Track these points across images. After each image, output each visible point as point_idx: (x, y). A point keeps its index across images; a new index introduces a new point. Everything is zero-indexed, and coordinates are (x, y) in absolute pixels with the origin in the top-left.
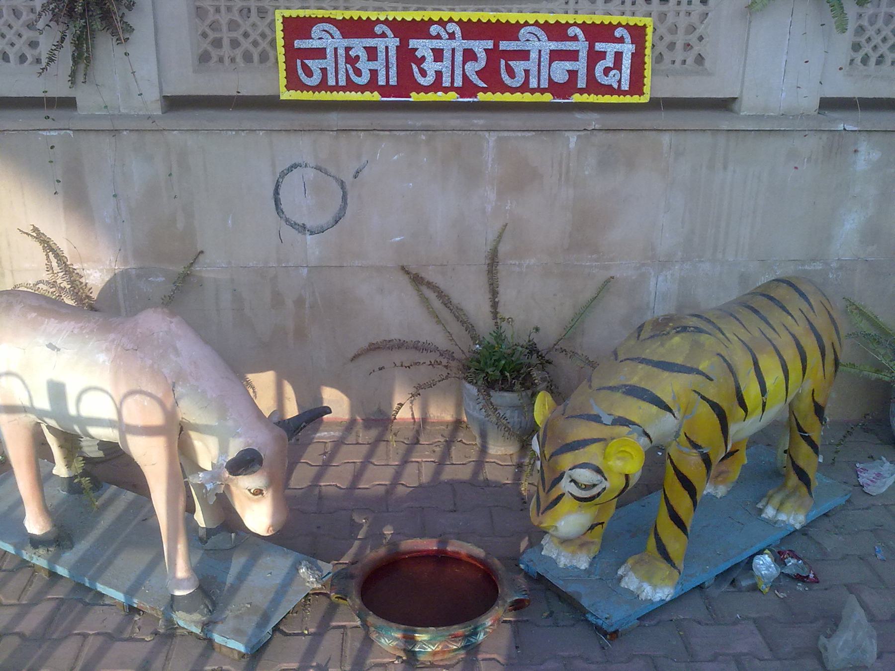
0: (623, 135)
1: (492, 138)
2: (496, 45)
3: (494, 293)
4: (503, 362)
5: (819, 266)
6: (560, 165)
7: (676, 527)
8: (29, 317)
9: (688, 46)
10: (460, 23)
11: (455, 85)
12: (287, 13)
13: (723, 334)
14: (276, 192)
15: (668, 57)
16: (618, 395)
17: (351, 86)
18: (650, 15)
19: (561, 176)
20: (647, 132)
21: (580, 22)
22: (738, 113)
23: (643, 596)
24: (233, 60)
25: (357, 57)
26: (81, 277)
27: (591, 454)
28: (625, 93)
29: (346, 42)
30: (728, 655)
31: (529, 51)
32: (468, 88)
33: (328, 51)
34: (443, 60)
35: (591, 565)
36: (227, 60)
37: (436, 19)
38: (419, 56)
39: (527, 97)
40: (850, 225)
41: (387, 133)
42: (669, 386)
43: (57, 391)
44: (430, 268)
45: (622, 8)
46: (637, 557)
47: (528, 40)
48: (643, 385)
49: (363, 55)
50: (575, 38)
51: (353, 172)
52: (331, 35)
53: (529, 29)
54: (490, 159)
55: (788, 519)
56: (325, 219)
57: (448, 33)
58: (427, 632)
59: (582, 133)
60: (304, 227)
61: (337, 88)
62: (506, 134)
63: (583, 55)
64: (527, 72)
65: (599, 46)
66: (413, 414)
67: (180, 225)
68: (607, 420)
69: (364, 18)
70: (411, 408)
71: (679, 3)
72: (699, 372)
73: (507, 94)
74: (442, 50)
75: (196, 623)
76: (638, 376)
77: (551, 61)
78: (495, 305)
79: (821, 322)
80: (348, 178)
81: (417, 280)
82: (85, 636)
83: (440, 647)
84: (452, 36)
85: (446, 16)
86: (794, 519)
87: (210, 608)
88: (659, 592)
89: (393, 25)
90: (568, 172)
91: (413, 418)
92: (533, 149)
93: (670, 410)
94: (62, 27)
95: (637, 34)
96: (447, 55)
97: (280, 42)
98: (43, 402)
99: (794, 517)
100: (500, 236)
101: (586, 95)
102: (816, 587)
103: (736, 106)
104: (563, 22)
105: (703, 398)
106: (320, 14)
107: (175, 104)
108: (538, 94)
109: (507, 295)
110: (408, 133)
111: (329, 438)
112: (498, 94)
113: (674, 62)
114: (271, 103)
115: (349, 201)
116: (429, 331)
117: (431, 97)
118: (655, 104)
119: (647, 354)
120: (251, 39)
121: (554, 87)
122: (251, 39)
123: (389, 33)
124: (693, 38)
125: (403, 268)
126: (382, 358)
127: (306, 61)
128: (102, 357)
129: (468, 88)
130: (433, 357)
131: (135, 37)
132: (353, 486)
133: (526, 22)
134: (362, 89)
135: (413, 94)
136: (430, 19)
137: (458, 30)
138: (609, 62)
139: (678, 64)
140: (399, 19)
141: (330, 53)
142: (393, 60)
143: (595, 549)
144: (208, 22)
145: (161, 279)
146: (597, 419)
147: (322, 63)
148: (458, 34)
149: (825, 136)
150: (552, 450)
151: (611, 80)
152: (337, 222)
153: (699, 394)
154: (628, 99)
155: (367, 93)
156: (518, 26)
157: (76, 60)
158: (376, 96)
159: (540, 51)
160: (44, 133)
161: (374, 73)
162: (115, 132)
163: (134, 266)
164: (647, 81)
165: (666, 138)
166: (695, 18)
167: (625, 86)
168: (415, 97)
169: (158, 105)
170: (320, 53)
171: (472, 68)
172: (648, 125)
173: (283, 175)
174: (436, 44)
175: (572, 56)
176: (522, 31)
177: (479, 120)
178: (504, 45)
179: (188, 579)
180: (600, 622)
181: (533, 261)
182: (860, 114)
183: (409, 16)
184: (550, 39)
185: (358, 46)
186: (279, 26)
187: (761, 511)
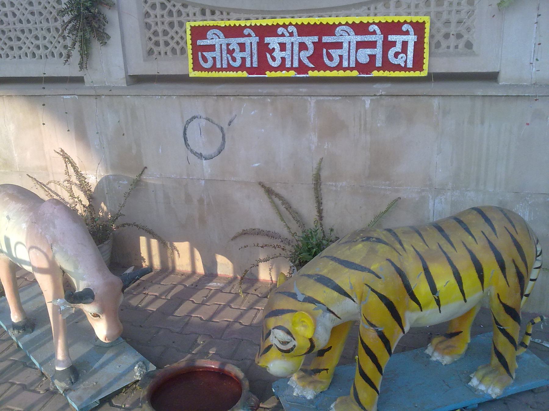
0: (403, 99)
1: (312, 101)
2: (320, 39)
3: (319, 203)
4: (315, 250)
6: (360, 120)
7: (364, 382)
9: (459, 36)
10: (296, 25)
11: (294, 66)
12: (193, 24)
13: (401, 245)
14: (185, 134)
15: (444, 44)
16: (311, 281)
17: (230, 68)
19: (360, 125)
21: (377, 21)
22: (498, 83)
25: (234, 50)
26: (86, 179)
27: (285, 320)
28: (409, 70)
31: (342, 42)
32: (302, 68)
34: (287, 50)
35: (316, 397)
37: (281, 23)
38: (271, 48)
39: (341, 74)
41: (247, 97)
42: (347, 279)
44: (278, 184)
46: (344, 397)
47: (341, 35)
48: (329, 276)
49: (237, 49)
50: (374, 33)
51: (228, 122)
54: (312, 115)
55: (487, 390)
56: (213, 150)
57: (289, 32)
59: (374, 98)
61: (222, 69)
62: (322, 98)
63: (380, 44)
64: (341, 57)
65: (391, 38)
66: (271, 278)
67: (134, 151)
68: (300, 297)
70: (270, 274)
71: (451, 4)
72: (370, 271)
73: (328, 72)
74: (285, 44)
75: (62, 387)
78: (320, 211)
79: (503, 243)
80: (225, 127)
82: (13, 384)
84: (291, 34)
85: (287, 21)
86: (492, 390)
87: (73, 381)
89: (255, 28)
90: (365, 124)
91: (272, 280)
92: (341, 108)
93: (349, 297)
95: (419, 28)
96: (288, 47)
97: (189, 42)
101: (381, 72)
104: (365, 22)
105: (373, 290)
106: (211, 23)
107: (138, 80)
108: (348, 72)
109: (328, 205)
111: (215, 287)
112: (322, 71)
114: (184, 79)
117: (279, 74)
118: (436, 77)
120: (175, 41)
121: (359, 67)
122: (175, 41)
123: (253, 34)
125: (260, 183)
126: (250, 240)
127: (204, 53)
129: (302, 68)
132: (210, 319)
133: (340, 23)
134: (236, 69)
135: (268, 73)
137: (295, 30)
138: (398, 48)
139: (452, 49)
140: (258, 25)
141: (217, 47)
142: (255, 51)
143: (322, 387)
144: (152, 31)
145: (126, 182)
146: (294, 296)
147: (213, 54)
148: (295, 33)
151: (400, 61)
152: (220, 153)
153: (368, 286)
154: (412, 74)
155: (240, 72)
156: (335, 26)
158: (245, 74)
159: (349, 42)
160: (65, 97)
161: (243, 59)
162: (97, 96)
164: (426, 61)
165: (436, 102)
167: (410, 65)
168: (268, 74)
169: (125, 81)
170: (211, 48)
171: (304, 55)
172: (420, 92)
173: (188, 123)
174: (281, 40)
175: (373, 45)
176: (338, 29)
177: (303, 89)
178: (326, 39)
179: (63, 361)
181: (344, 183)
183: (264, 23)
184: (356, 34)
185: (234, 42)
186: (189, 32)
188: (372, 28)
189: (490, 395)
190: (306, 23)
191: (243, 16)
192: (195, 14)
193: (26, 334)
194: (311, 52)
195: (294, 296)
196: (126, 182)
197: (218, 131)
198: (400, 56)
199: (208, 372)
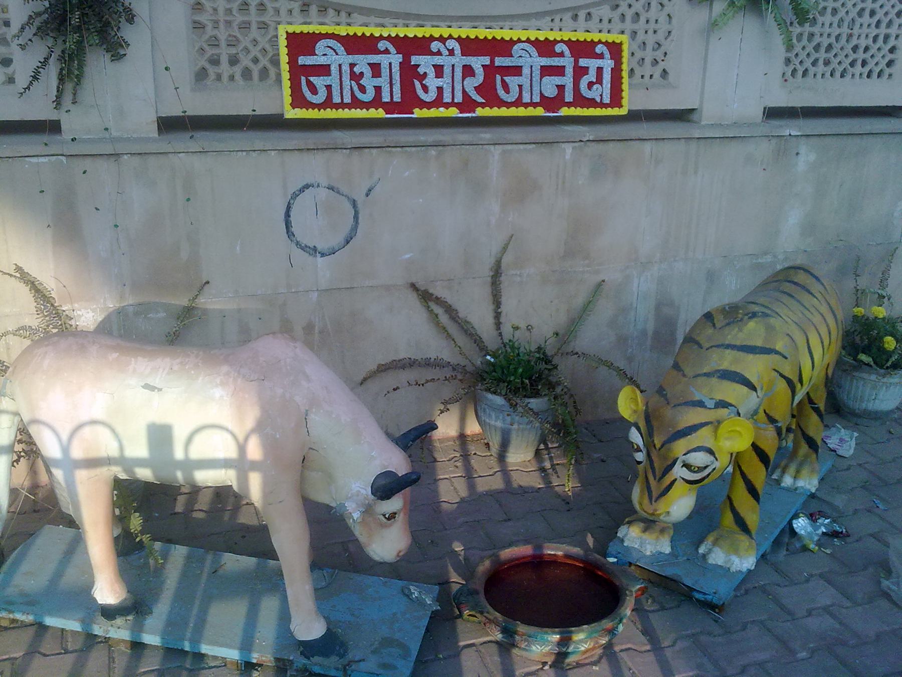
2: (492, 61)
3: (497, 303)
5: (769, 258)
8: (110, 358)
10: (459, 39)
11: (456, 101)
12: (291, 29)
14: (287, 215)
16: (714, 380)
17: (356, 103)
18: (623, 32)
20: (633, 142)
21: (566, 39)
23: (733, 569)
24: (232, 78)
25: (362, 74)
27: (703, 437)
29: (351, 59)
30: (819, 608)
33: (332, 68)
34: (446, 78)
36: (225, 78)
37: (437, 36)
40: (793, 219)
41: (399, 149)
42: (755, 367)
43: (160, 435)
45: (600, 26)
48: (733, 369)
49: (368, 72)
50: (561, 55)
51: (365, 191)
52: (335, 50)
53: (522, 45)
56: (336, 239)
58: (583, 631)
60: (315, 249)
61: (342, 106)
62: (509, 147)
63: (569, 71)
65: (583, 62)
68: (710, 404)
69: (359, 34)
74: (443, 66)
76: (727, 360)
77: (542, 77)
78: (497, 315)
80: (360, 198)
81: (426, 297)
83: (592, 644)
84: (451, 52)
86: (809, 484)
88: (744, 562)
89: (395, 41)
94: (50, 42)
95: (615, 49)
96: (447, 71)
97: (284, 59)
98: (139, 449)
99: (809, 483)
100: (505, 249)
102: (848, 540)
103: (695, 117)
104: (552, 39)
105: (782, 375)
106: (324, 29)
107: (169, 125)
108: (531, 109)
109: (509, 305)
110: (419, 148)
112: (496, 108)
113: (642, 77)
115: (360, 218)
116: (436, 348)
117: (433, 113)
118: (634, 116)
119: (729, 340)
123: (392, 49)
124: (659, 55)
127: (312, 79)
128: (218, 392)
129: (467, 104)
130: (448, 372)
131: (130, 51)
133: (519, 39)
135: (416, 110)
136: (431, 35)
138: (592, 76)
140: (402, 35)
141: (334, 69)
145: (162, 315)
146: (701, 404)
147: (327, 80)
148: (458, 51)
149: (774, 141)
150: (664, 439)
152: (348, 243)
155: (372, 110)
156: (512, 43)
157: (61, 79)
158: (380, 113)
162: (116, 156)
163: (131, 302)
164: (625, 94)
165: (647, 147)
166: (660, 36)
167: (607, 100)
168: (418, 113)
170: (324, 70)
172: (634, 135)
173: (295, 196)
174: (437, 60)
175: (559, 71)
176: (515, 47)
178: (499, 61)
180: (709, 598)
182: (801, 122)
183: (411, 32)
185: (363, 62)
186: (283, 42)
187: (778, 482)
188: (558, 48)
189: (809, 490)
190: (473, 37)
191: (373, 19)
192: (290, 11)
193: (145, 619)
194: (480, 78)
195: (701, 404)
196: (162, 315)
197: (348, 206)
198: (595, 87)
199: (520, 564)
